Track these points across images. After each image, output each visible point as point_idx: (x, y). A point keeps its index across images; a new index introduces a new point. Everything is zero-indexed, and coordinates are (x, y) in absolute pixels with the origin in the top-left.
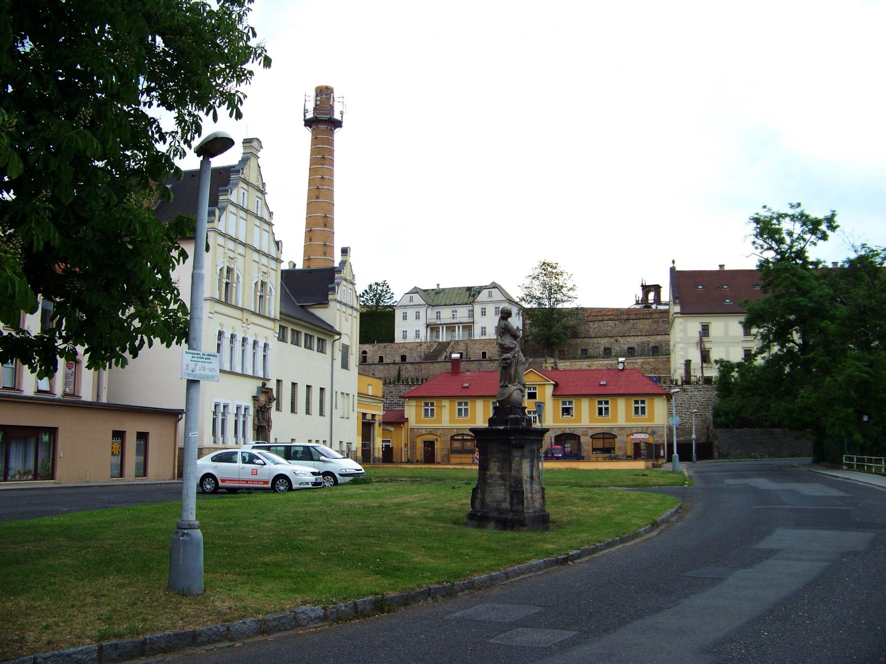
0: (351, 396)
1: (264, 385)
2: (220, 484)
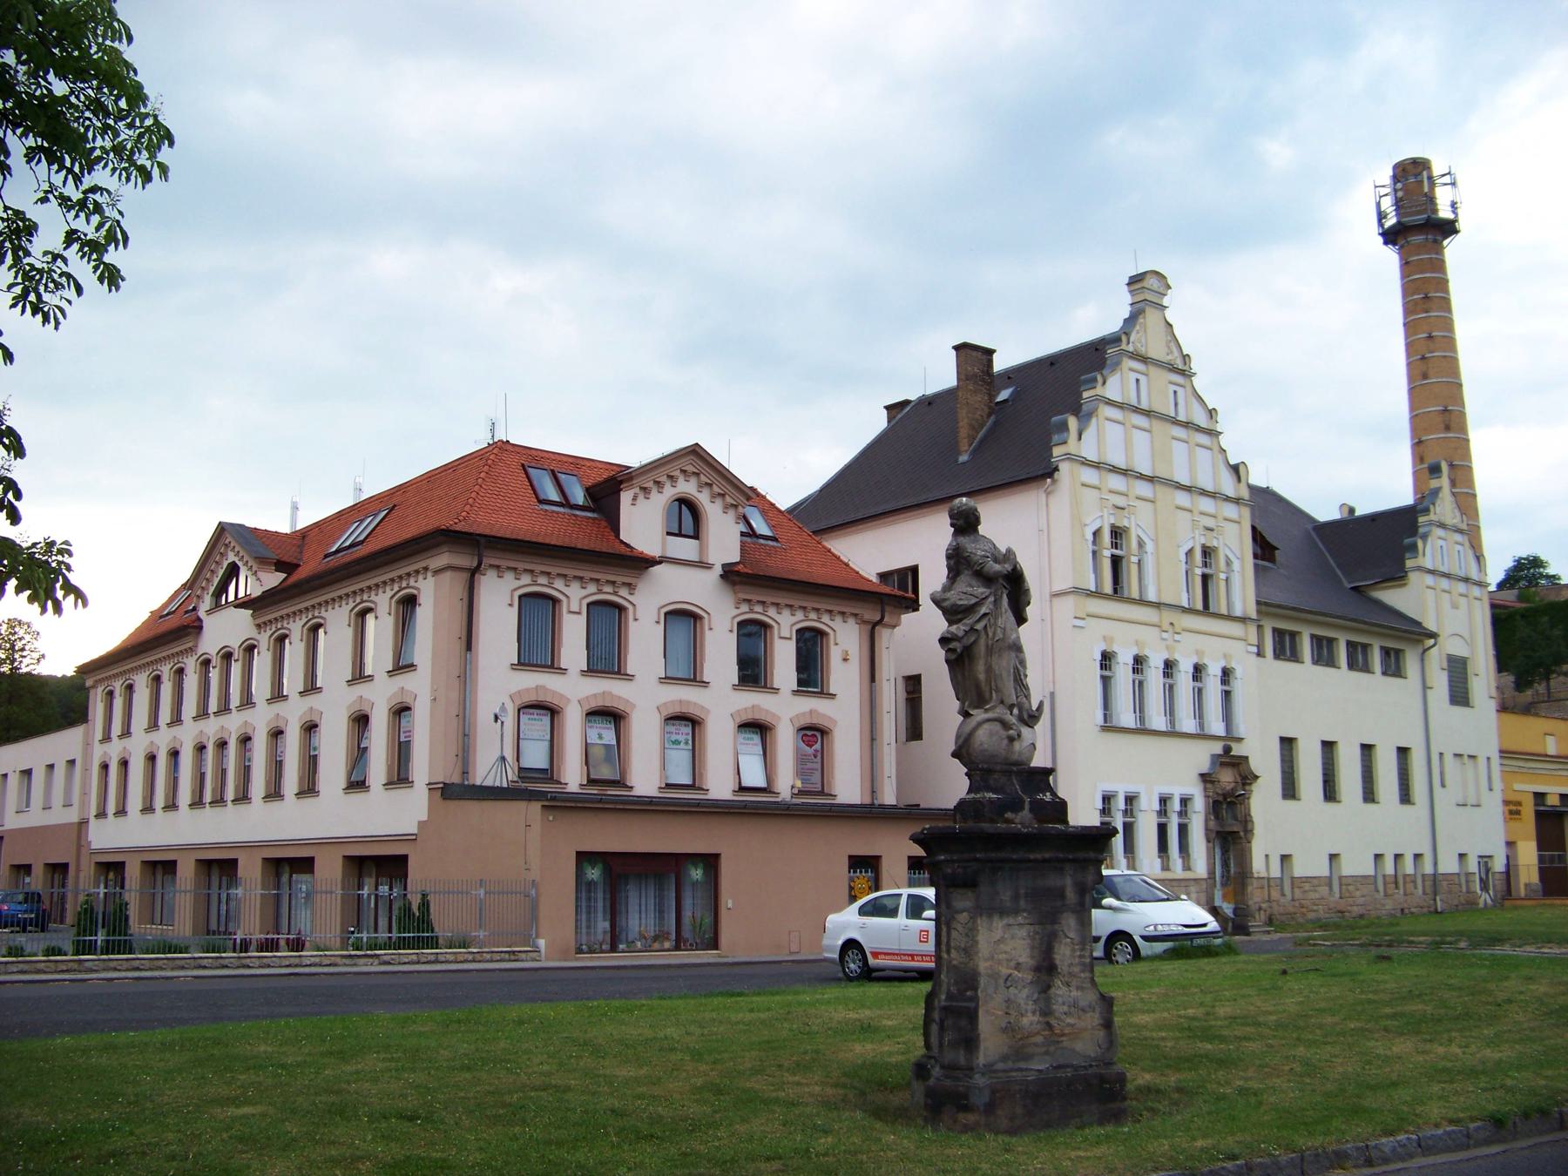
0: (1482, 762)
1: (1227, 750)
2: (871, 961)
